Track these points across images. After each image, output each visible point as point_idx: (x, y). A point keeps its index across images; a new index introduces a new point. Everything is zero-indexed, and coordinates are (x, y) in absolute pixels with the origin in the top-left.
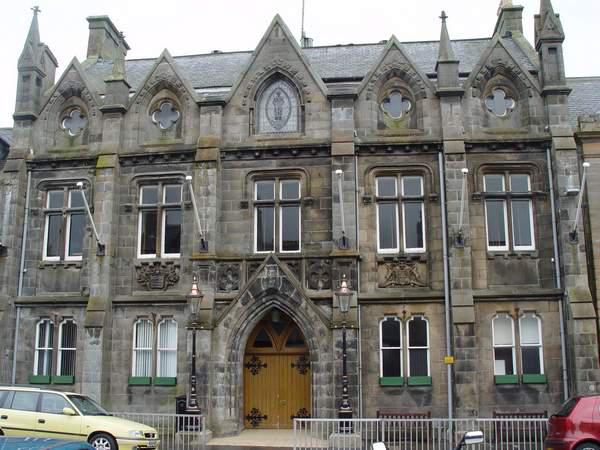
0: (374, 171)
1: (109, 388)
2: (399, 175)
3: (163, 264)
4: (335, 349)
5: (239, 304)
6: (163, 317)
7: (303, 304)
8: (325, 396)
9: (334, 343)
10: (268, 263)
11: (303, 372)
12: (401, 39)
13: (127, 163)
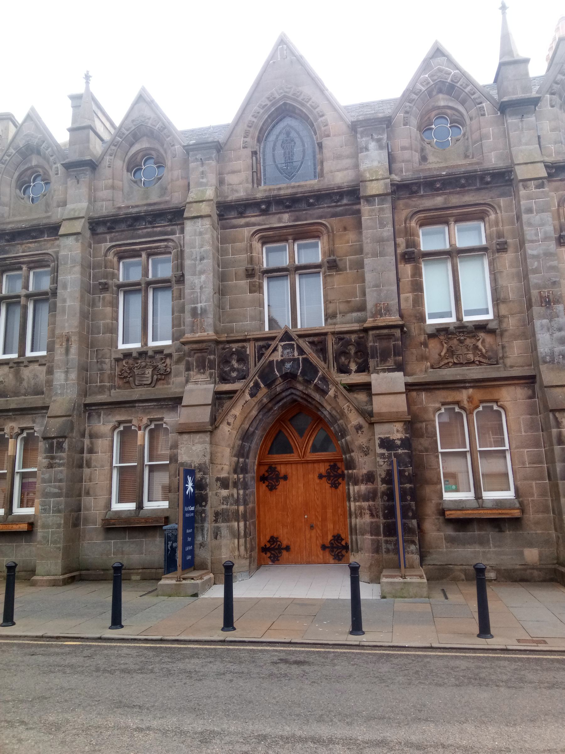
0: (416, 218)
1: (78, 519)
2: (452, 219)
3: (150, 353)
4: (379, 451)
5: (248, 397)
6: (151, 420)
7: (331, 393)
8: (367, 519)
9: (377, 442)
10: (282, 340)
11: (335, 486)
12: (69, 125)
13: (101, 229)
